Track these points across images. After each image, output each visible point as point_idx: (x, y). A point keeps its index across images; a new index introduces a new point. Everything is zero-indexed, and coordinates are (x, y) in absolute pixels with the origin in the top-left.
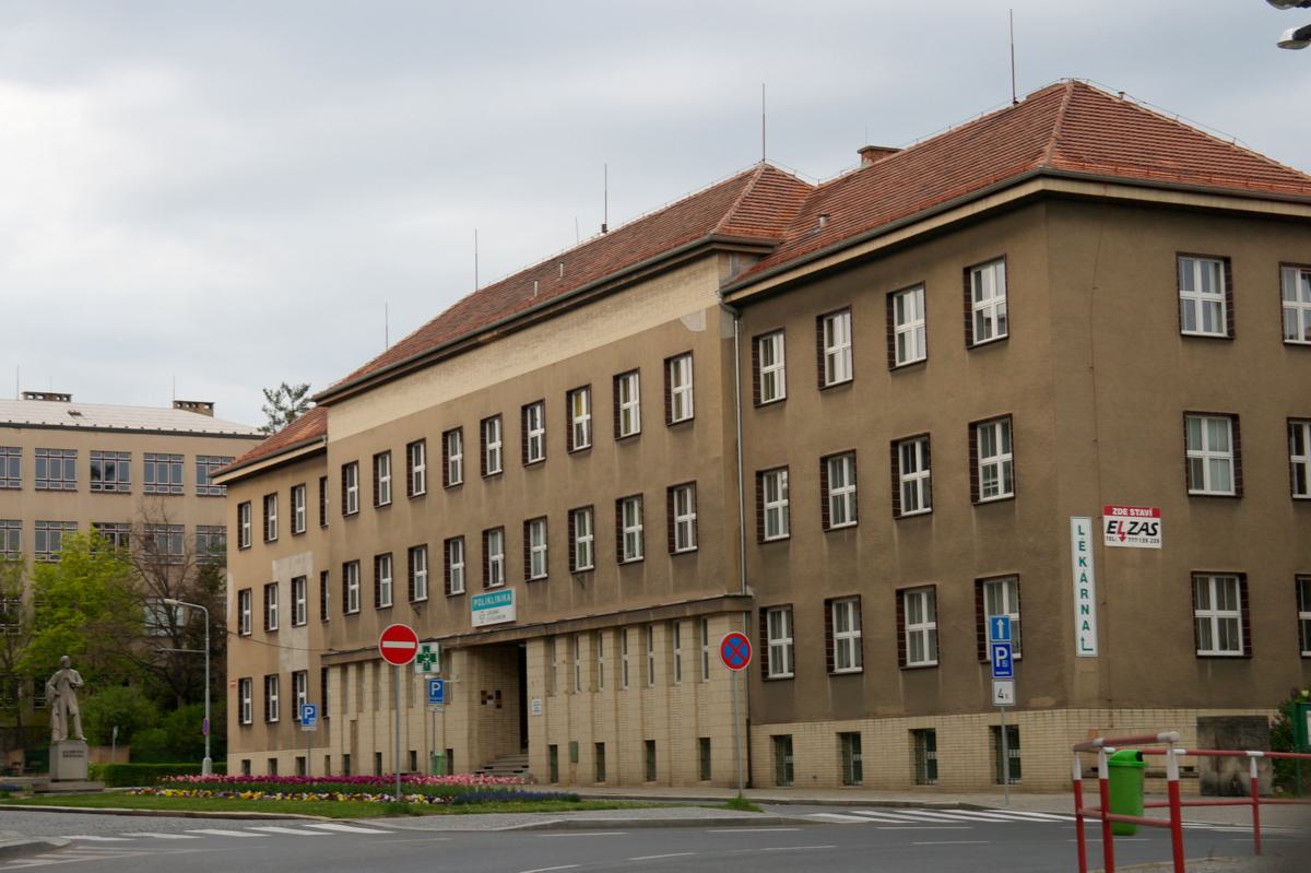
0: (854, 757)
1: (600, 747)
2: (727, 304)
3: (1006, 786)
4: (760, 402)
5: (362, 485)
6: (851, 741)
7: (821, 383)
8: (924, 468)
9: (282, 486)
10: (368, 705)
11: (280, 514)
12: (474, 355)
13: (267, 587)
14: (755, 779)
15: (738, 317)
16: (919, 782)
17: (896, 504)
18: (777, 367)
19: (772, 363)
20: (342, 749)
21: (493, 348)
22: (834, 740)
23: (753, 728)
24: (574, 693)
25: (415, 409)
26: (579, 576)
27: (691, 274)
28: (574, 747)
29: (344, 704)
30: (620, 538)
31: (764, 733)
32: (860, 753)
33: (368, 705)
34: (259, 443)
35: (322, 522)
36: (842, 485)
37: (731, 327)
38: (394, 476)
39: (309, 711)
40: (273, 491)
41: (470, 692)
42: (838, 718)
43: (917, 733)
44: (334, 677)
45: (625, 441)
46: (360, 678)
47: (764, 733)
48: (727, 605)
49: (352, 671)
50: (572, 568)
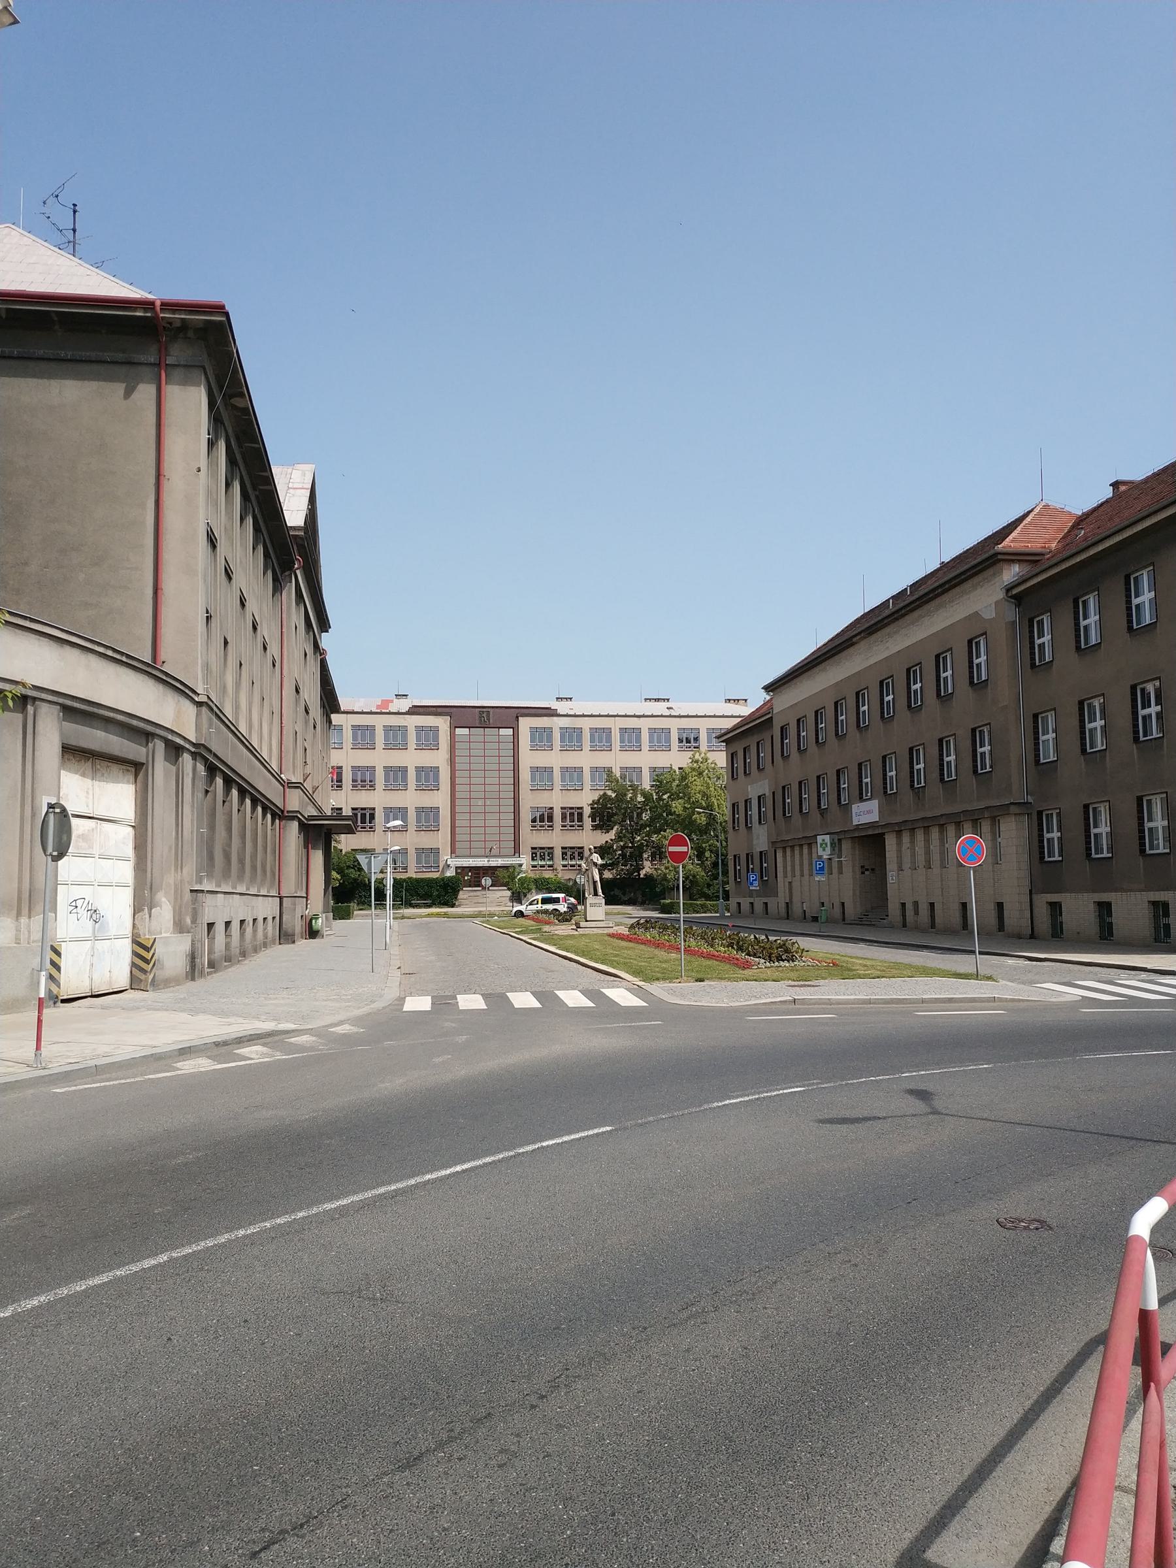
0: (1164, 921)
1: (932, 905)
2: (1011, 597)
3: (390, 912)
4: (1035, 665)
5: (791, 740)
6: (1105, 908)
7: (1130, 628)
8: (1157, 705)
9: (752, 741)
10: (798, 873)
11: (752, 759)
12: (851, 650)
13: (746, 801)
14: (1036, 933)
15: (1018, 605)
16: (1157, 940)
17: (1136, 732)
18: (1093, 619)
19: (1043, 636)
20: (785, 900)
21: (863, 645)
22: (1092, 907)
23: (1034, 896)
24: (916, 869)
25: (1165, 516)
26: (916, 790)
27: (984, 579)
28: (916, 904)
29: (785, 872)
30: (942, 765)
31: (1042, 900)
32: (1111, 916)
33: (798, 873)
34: (741, 719)
35: (773, 762)
36: (1150, 706)
37: (1011, 613)
38: (807, 733)
39: (753, 877)
40: (734, 751)
41: (853, 866)
42: (1094, 891)
43: (1154, 904)
44: (779, 855)
45: (944, 698)
46: (793, 856)
47: (1042, 900)
48: (1013, 809)
49: (788, 851)
50: (912, 786)
